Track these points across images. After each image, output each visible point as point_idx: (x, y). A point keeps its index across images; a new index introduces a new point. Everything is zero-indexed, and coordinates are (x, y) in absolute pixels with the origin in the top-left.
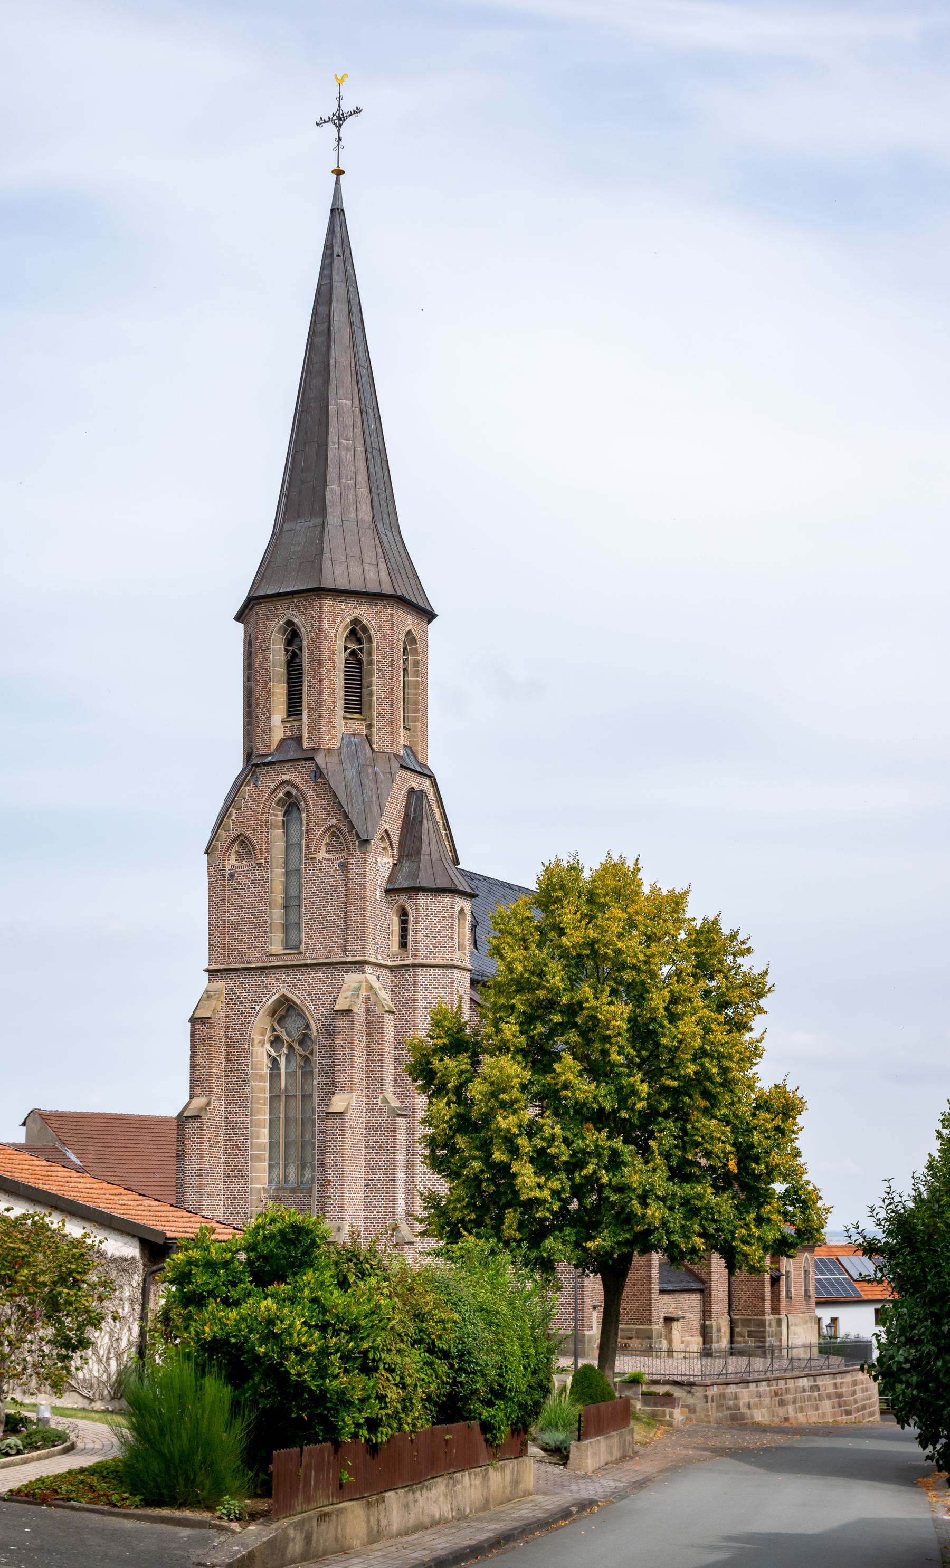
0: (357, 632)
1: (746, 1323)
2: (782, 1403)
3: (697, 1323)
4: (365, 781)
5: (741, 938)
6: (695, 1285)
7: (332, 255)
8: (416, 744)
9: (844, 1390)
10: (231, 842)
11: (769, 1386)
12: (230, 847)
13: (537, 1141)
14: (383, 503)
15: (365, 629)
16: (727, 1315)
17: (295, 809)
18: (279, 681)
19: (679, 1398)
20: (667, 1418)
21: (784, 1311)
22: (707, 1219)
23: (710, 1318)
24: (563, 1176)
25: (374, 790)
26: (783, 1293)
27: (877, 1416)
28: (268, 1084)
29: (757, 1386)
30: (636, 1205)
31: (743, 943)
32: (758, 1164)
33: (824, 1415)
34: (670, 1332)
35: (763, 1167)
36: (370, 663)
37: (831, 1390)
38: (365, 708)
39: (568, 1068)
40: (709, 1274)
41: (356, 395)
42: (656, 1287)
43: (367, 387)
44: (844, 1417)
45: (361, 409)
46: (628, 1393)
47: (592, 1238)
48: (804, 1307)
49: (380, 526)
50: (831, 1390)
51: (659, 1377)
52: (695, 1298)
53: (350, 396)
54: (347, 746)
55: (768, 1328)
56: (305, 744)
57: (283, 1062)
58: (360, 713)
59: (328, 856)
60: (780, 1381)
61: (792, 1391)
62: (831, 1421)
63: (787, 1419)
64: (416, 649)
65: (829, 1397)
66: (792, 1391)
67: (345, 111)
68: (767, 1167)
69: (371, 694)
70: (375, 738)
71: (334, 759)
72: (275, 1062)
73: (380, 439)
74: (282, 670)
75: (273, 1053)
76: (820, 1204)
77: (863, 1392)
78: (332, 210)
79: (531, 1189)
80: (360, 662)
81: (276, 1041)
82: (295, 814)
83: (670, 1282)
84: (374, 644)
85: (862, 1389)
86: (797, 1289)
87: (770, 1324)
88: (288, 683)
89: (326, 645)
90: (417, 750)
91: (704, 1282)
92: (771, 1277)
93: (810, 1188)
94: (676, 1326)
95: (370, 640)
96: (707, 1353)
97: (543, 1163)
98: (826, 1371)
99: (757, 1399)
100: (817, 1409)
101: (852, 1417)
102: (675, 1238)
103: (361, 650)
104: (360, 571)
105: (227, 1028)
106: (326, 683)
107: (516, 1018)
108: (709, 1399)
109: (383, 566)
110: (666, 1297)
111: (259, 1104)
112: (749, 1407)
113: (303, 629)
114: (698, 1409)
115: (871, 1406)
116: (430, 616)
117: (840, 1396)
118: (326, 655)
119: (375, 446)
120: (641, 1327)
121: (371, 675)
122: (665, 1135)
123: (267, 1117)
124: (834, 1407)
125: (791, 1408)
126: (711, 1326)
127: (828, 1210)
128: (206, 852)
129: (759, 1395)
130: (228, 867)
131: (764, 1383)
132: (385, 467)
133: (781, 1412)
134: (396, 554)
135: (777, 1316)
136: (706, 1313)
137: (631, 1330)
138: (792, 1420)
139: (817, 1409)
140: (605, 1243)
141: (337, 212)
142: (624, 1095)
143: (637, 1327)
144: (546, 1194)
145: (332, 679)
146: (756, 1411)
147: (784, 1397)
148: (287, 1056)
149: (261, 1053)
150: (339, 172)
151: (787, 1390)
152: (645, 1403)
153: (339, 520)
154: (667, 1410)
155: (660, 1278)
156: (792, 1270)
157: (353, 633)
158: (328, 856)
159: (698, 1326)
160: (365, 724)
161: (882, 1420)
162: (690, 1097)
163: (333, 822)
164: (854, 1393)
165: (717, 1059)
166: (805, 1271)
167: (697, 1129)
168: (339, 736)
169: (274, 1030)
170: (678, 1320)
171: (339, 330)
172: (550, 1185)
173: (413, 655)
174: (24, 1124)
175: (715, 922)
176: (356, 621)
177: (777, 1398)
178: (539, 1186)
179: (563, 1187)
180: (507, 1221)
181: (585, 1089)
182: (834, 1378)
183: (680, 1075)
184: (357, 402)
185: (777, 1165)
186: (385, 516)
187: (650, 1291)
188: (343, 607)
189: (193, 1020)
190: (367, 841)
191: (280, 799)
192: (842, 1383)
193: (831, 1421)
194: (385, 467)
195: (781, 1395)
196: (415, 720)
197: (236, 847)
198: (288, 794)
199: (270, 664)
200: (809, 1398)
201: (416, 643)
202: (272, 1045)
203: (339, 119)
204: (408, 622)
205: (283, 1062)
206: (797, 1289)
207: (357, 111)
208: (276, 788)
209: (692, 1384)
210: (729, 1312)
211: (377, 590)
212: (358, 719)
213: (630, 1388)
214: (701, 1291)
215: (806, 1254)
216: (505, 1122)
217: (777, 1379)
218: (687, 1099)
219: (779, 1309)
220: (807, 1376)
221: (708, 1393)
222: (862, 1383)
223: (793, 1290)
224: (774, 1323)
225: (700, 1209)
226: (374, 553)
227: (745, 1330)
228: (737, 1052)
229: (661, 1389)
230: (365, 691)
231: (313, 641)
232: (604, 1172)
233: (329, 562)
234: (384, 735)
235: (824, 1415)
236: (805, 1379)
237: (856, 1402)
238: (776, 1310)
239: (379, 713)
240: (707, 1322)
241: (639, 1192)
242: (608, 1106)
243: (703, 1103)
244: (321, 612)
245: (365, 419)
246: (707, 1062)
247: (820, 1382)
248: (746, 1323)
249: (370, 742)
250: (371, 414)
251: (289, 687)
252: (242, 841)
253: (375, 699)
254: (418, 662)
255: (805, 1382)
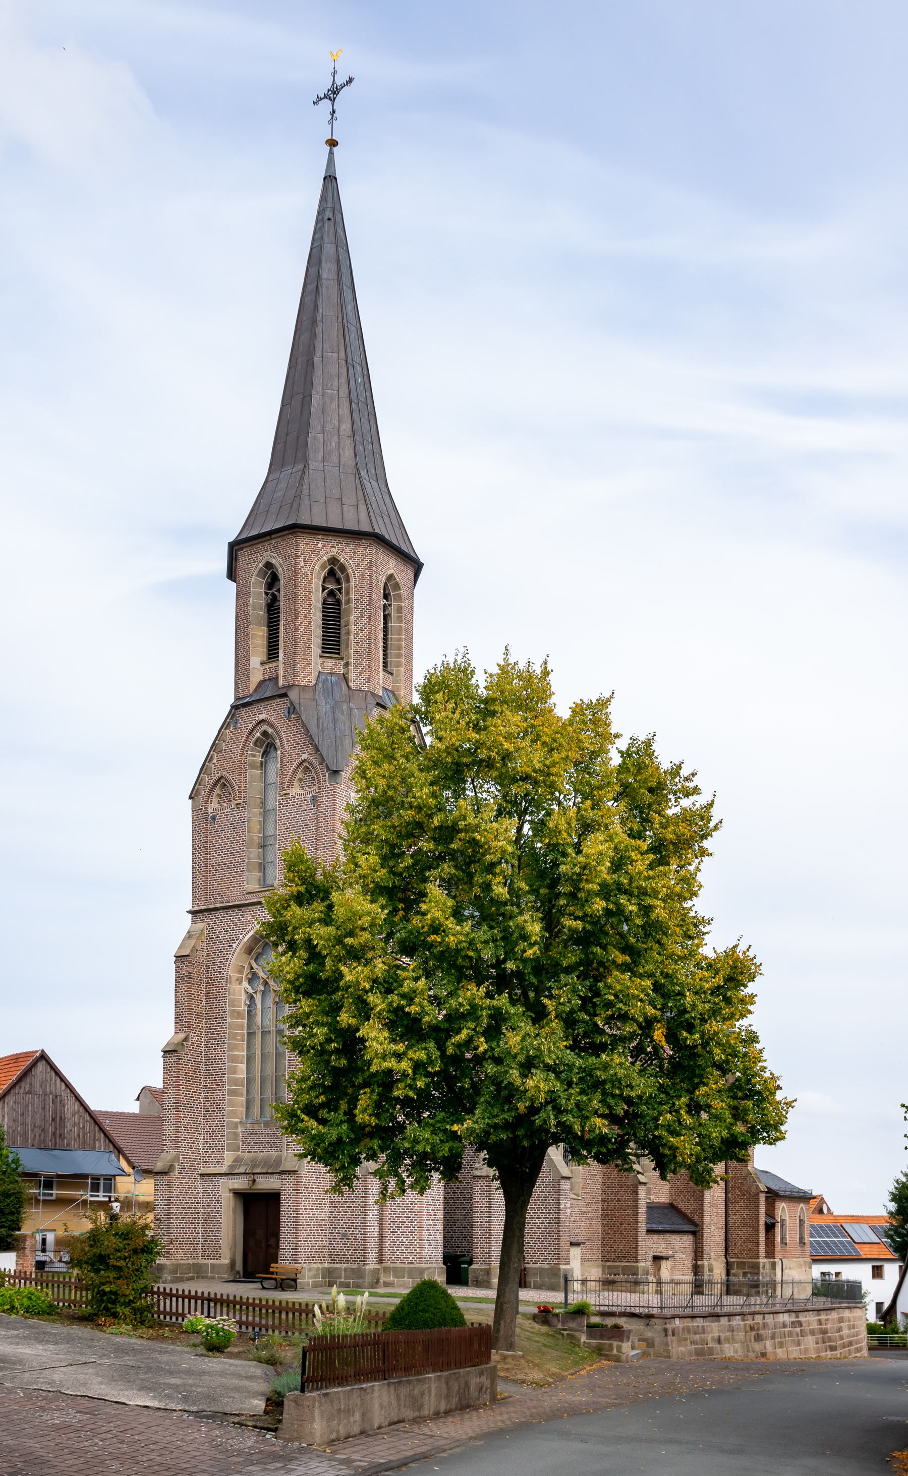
0: (335, 573)
1: (741, 1265)
2: (758, 1338)
3: (688, 1263)
4: (338, 715)
5: (684, 772)
6: (692, 1228)
7: (323, 219)
8: (399, 688)
9: (829, 1326)
10: (213, 786)
11: (743, 1320)
12: (212, 790)
13: (394, 998)
14: (369, 453)
15: (343, 568)
16: (723, 1259)
17: (272, 748)
18: (259, 624)
19: (630, 1331)
20: (615, 1352)
21: (778, 1255)
22: (613, 1096)
23: (702, 1259)
24: (431, 1045)
25: (347, 723)
26: (778, 1239)
27: (865, 1352)
28: (246, 1021)
29: (729, 1321)
30: (515, 1074)
31: (687, 779)
32: (691, 1034)
33: (806, 1350)
34: (659, 1270)
35: (697, 1036)
36: (348, 602)
37: (815, 1326)
38: (343, 647)
39: (437, 902)
40: (702, 1217)
41: (342, 348)
42: (643, 1227)
43: (355, 343)
44: (829, 1353)
45: (346, 361)
46: (572, 1325)
47: (461, 1121)
48: (799, 1252)
49: (363, 473)
50: (815, 1326)
51: (615, 1309)
52: (686, 1241)
53: (336, 349)
54: (323, 684)
55: (761, 1270)
56: (281, 683)
57: (258, 998)
58: (338, 653)
59: (301, 792)
60: (756, 1316)
61: (771, 1326)
62: (814, 1356)
63: (764, 1355)
64: (399, 595)
65: (813, 1332)
66: (771, 1326)
67: (339, 84)
68: (702, 1037)
69: (348, 633)
70: (351, 676)
71: (309, 695)
72: (251, 998)
73: (368, 394)
74: (262, 613)
75: (251, 991)
76: (779, 1096)
77: (849, 1329)
78: (325, 178)
79: (384, 1057)
80: (338, 602)
81: (253, 978)
82: (272, 754)
83: (660, 1223)
84: (352, 583)
85: (849, 1326)
86: (792, 1236)
87: (764, 1266)
88: (269, 627)
89: (302, 582)
90: (399, 695)
91: (696, 1225)
92: (766, 1224)
93: (767, 1075)
94: (664, 1264)
95: (348, 580)
96: (698, 1287)
97: (405, 1026)
98: (809, 1307)
99: (729, 1334)
100: (799, 1344)
101: (838, 1352)
102: (568, 1118)
103: (340, 590)
104: (339, 511)
105: (207, 967)
106: (301, 620)
107: (377, 848)
108: (670, 1332)
109: (362, 507)
110: (655, 1237)
111: (237, 1040)
112: (719, 1341)
113: (280, 569)
114: (656, 1344)
115: (858, 1342)
116: (417, 566)
117: (824, 1332)
118: (301, 593)
119: (362, 399)
120: (627, 1264)
121: (349, 614)
122: (564, 995)
123: (245, 1053)
124: (817, 1343)
125: (769, 1344)
126: (703, 1266)
127: (789, 1104)
128: (190, 798)
129: (732, 1330)
130: (210, 810)
131: (738, 1317)
132: (372, 421)
133: (758, 1347)
134: (381, 502)
135: (772, 1260)
136: (698, 1253)
137: (617, 1267)
138: (771, 1357)
139: (799, 1344)
140: (476, 1126)
141: (330, 180)
142: (510, 940)
143: (623, 1264)
144: (405, 1065)
145: (308, 617)
146: (727, 1345)
147: (761, 1332)
148: (264, 993)
149: (239, 991)
150: (332, 143)
151: (765, 1326)
152: (591, 1336)
153: (321, 465)
154: (615, 1344)
155: (648, 1219)
156: (787, 1219)
157: (331, 573)
158: (301, 792)
159: (690, 1266)
160: (342, 663)
161: (871, 1356)
162: (604, 948)
163: (305, 756)
164: (840, 1330)
165: (638, 896)
166: (801, 1221)
167: (610, 987)
168: (314, 674)
169: (252, 968)
170: (667, 1258)
171: (328, 288)
172: (411, 1054)
173: (396, 600)
174: (138, 1099)
175: (648, 743)
176: (333, 560)
177: (753, 1333)
178: (399, 1056)
179: (429, 1058)
180: (361, 1104)
181: (457, 933)
182: (819, 1315)
183: (585, 915)
184: (342, 354)
185: (716, 1033)
186: (371, 466)
187: (636, 1230)
188: (320, 545)
189: (180, 958)
190: (336, 773)
191: (258, 739)
192: (827, 1320)
193: (814, 1356)
194: (372, 421)
195: (758, 1329)
196: (398, 665)
197: (217, 790)
198: (265, 733)
199: (250, 607)
200: (790, 1334)
201: (399, 589)
202: (249, 983)
203: (333, 93)
204: (391, 566)
205: (258, 998)
206: (792, 1236)
207: (350, 80)
208: (252, 731)
209: (650, 1316)
210: (726, 1256)
211: (355, 528)
212: (336, 658)
213: (574, 1319)
214: (694, 1233)
215: (802, 1205)
216: (351, 974)
217: (754, 1313)
218: (598, 950)
219: (773, 1253)
220: (788, 1311)
221: (668, 1326)
222: (849, 1321)
223: (787, 1237)
224: (768, 1266)
225: (604, 1082)
226: (355, 496)
227: (741, 1272)
228: (663, 887)
229: (609, 1322)
230: (343, 631)
231: (290, 579)
232: (482, 1039)
233: (307, 502)
234: (361, 673)
235: (806, 1350)
236: (786, 1315)
237: (841, 1338)
238: (770, 1254)
239: (356, 652)
240: (699, 1263)
241: (521, 1058)
242: (487, 954)
243: (621, 958)
244: (297, 550)
245: (351, 371)
246: (623, 900)
247: (802, 1318)
248: (741, 1265)
249: (346, 680)
250: (359, 368)
251: (270, 631)
252: (222, 783)
253: (352, 637)
254: (401, 607)
255: (786, 1318)
